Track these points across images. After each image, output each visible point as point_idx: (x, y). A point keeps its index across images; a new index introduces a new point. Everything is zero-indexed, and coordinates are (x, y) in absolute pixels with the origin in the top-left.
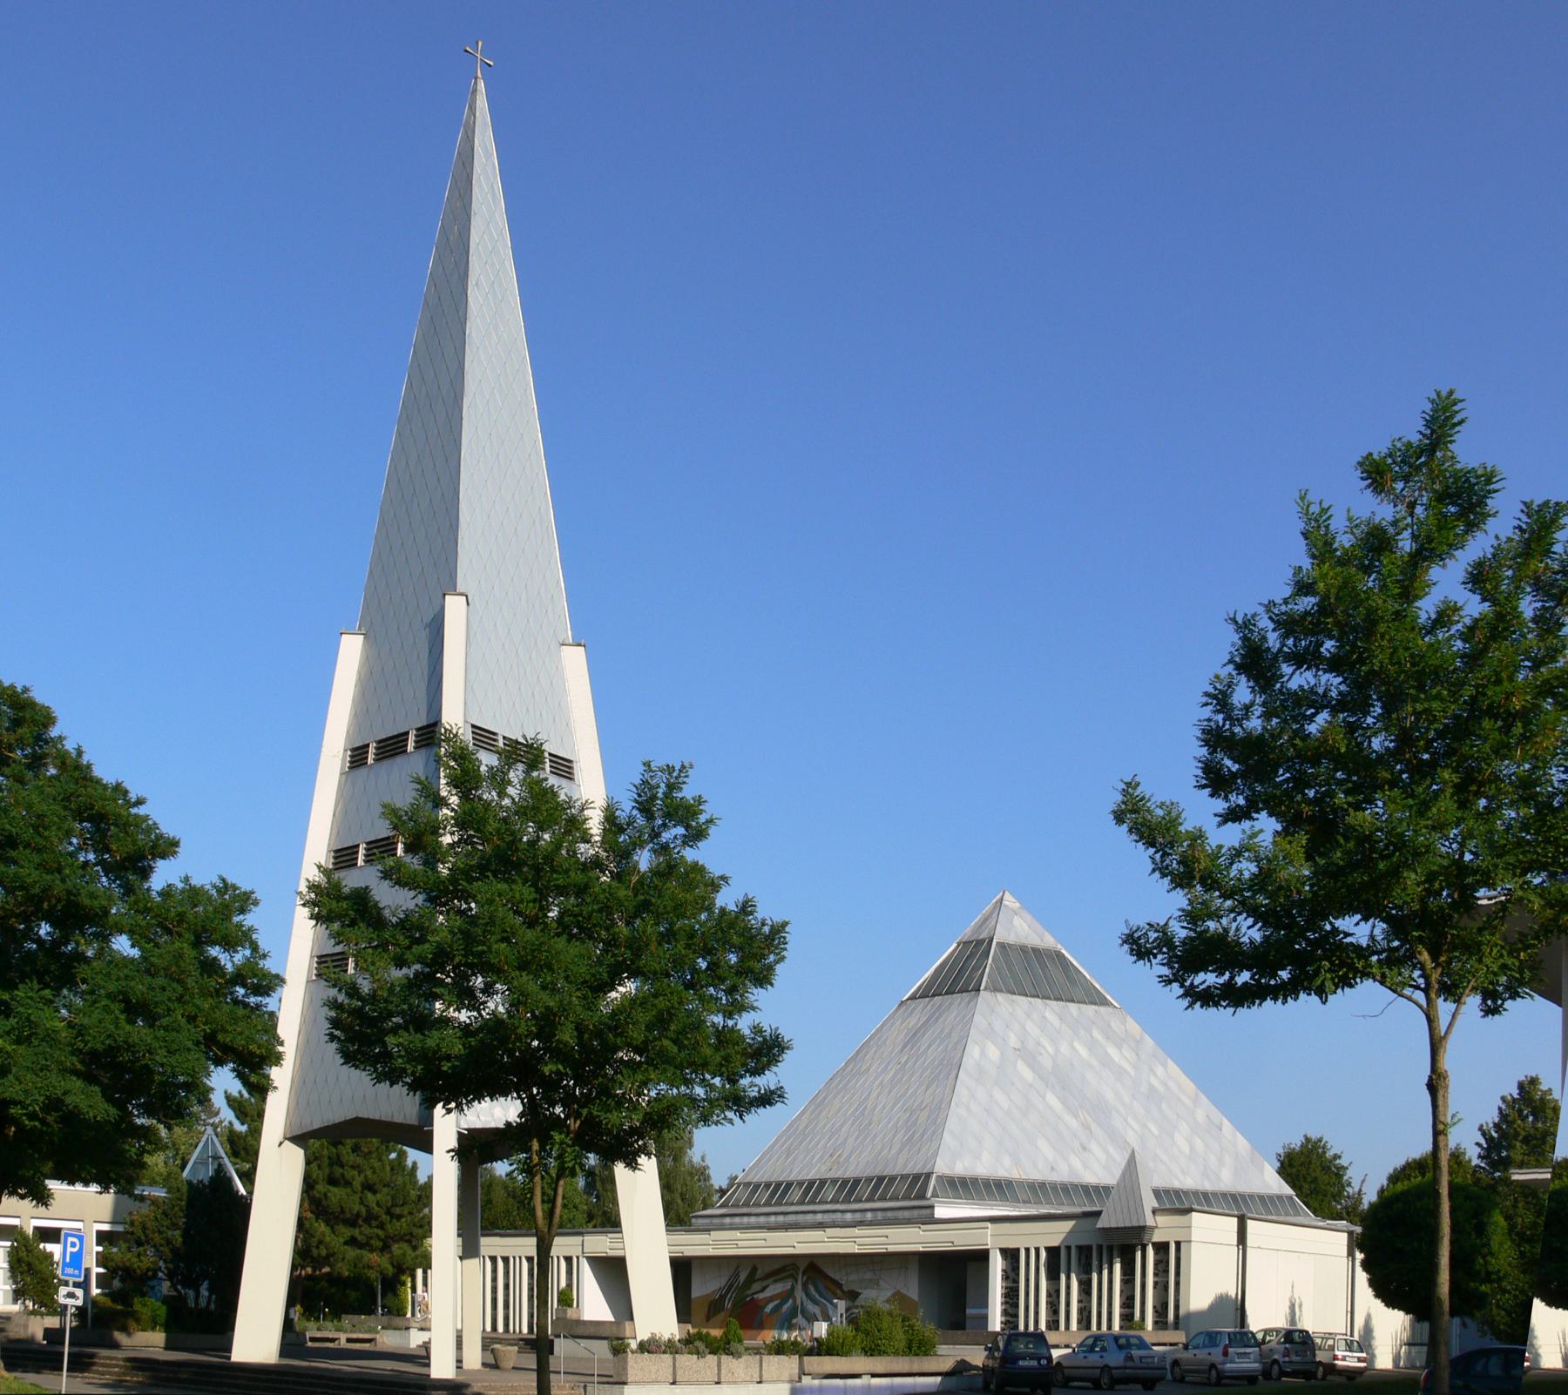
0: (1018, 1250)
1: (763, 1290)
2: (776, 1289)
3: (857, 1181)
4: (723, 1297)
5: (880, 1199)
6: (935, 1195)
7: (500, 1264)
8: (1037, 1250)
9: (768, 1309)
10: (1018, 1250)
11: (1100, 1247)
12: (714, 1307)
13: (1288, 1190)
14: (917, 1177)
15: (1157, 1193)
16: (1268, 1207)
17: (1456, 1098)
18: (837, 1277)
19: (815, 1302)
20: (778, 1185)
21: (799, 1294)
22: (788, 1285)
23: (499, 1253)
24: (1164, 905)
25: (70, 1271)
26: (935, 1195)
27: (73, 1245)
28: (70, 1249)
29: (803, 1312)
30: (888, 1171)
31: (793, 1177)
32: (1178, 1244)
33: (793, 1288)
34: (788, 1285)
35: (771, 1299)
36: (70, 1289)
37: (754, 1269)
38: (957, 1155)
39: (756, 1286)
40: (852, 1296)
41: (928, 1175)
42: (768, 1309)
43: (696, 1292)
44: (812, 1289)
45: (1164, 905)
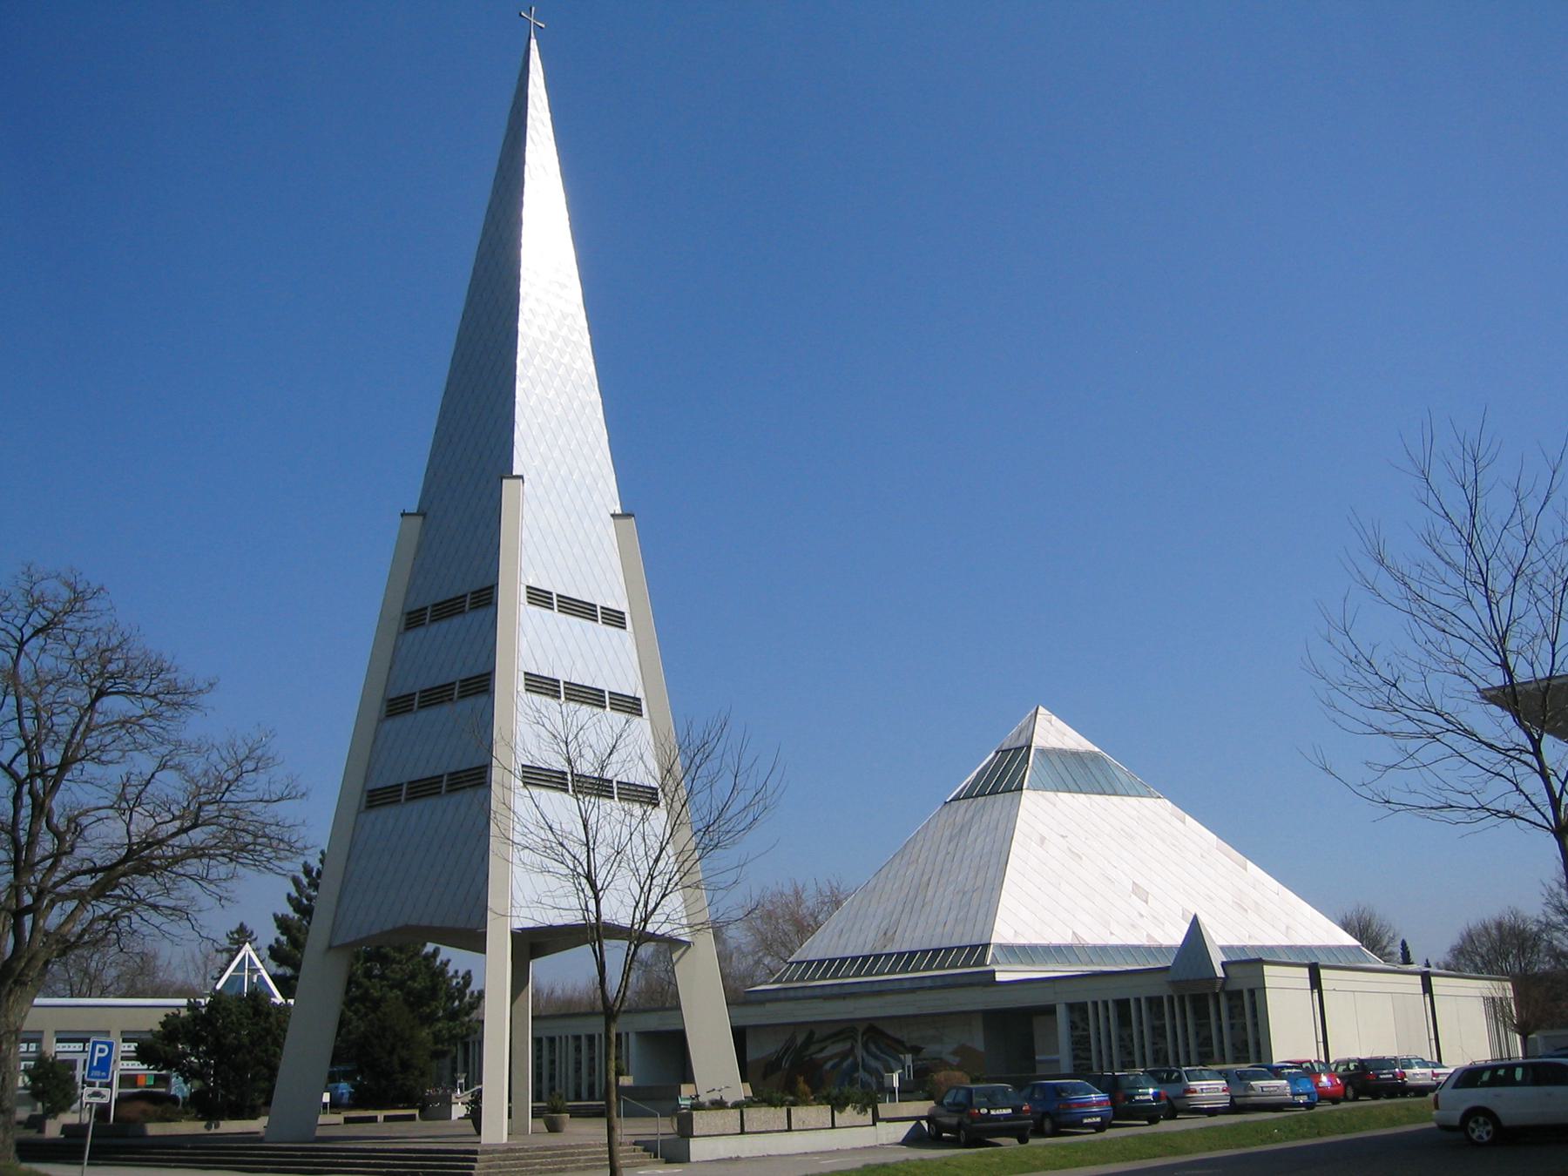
0: (1128, 1001)
1: (822, 1050)
2: (838, 1048)
3: (913, 954)
4: (779, 1059)
5: (938, 968)
6: (995, 961)
7: (545, 1043)
8: (1106, 1003)
9: (828, 1066)
10: (1128, 1001)
11: (1171, 999)
12: (771, 1067)
13: (1357, 943)
14: (974, 948)
15: (1222, 948)
16: (1342, 961)
17: (608, 986)
18: (898, 1036)
19: (876, 1057)
20: (832, 961)
21: (860, 1052)
22: (848, 1045)
23: (583, 1032)
24: (295, 894)
25: (97, 1073)
26: (995, 961)
27: (101, 1051)
28: (97, 1055)
29: (864, 1066)
30: (946, 944)
31: (849, 952)
32: (1252, 992)
33: (852, 1048)
34: (848, 1045)
35: (830, 1058)
36: (97, 1089)
37: (811, 1034)
38: (1005, 931)
39: (813, 1048)
40: (916, 1050)
41: (986, 946)
42: (828, 1066)
43: (752, 1055)
44: (873, 1048)
45: (295, 894)
